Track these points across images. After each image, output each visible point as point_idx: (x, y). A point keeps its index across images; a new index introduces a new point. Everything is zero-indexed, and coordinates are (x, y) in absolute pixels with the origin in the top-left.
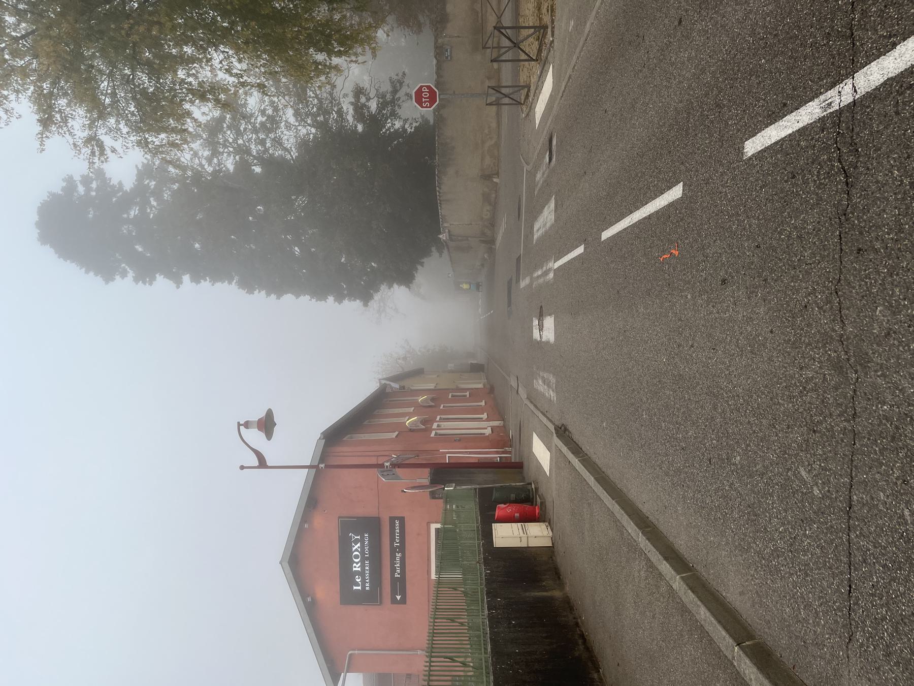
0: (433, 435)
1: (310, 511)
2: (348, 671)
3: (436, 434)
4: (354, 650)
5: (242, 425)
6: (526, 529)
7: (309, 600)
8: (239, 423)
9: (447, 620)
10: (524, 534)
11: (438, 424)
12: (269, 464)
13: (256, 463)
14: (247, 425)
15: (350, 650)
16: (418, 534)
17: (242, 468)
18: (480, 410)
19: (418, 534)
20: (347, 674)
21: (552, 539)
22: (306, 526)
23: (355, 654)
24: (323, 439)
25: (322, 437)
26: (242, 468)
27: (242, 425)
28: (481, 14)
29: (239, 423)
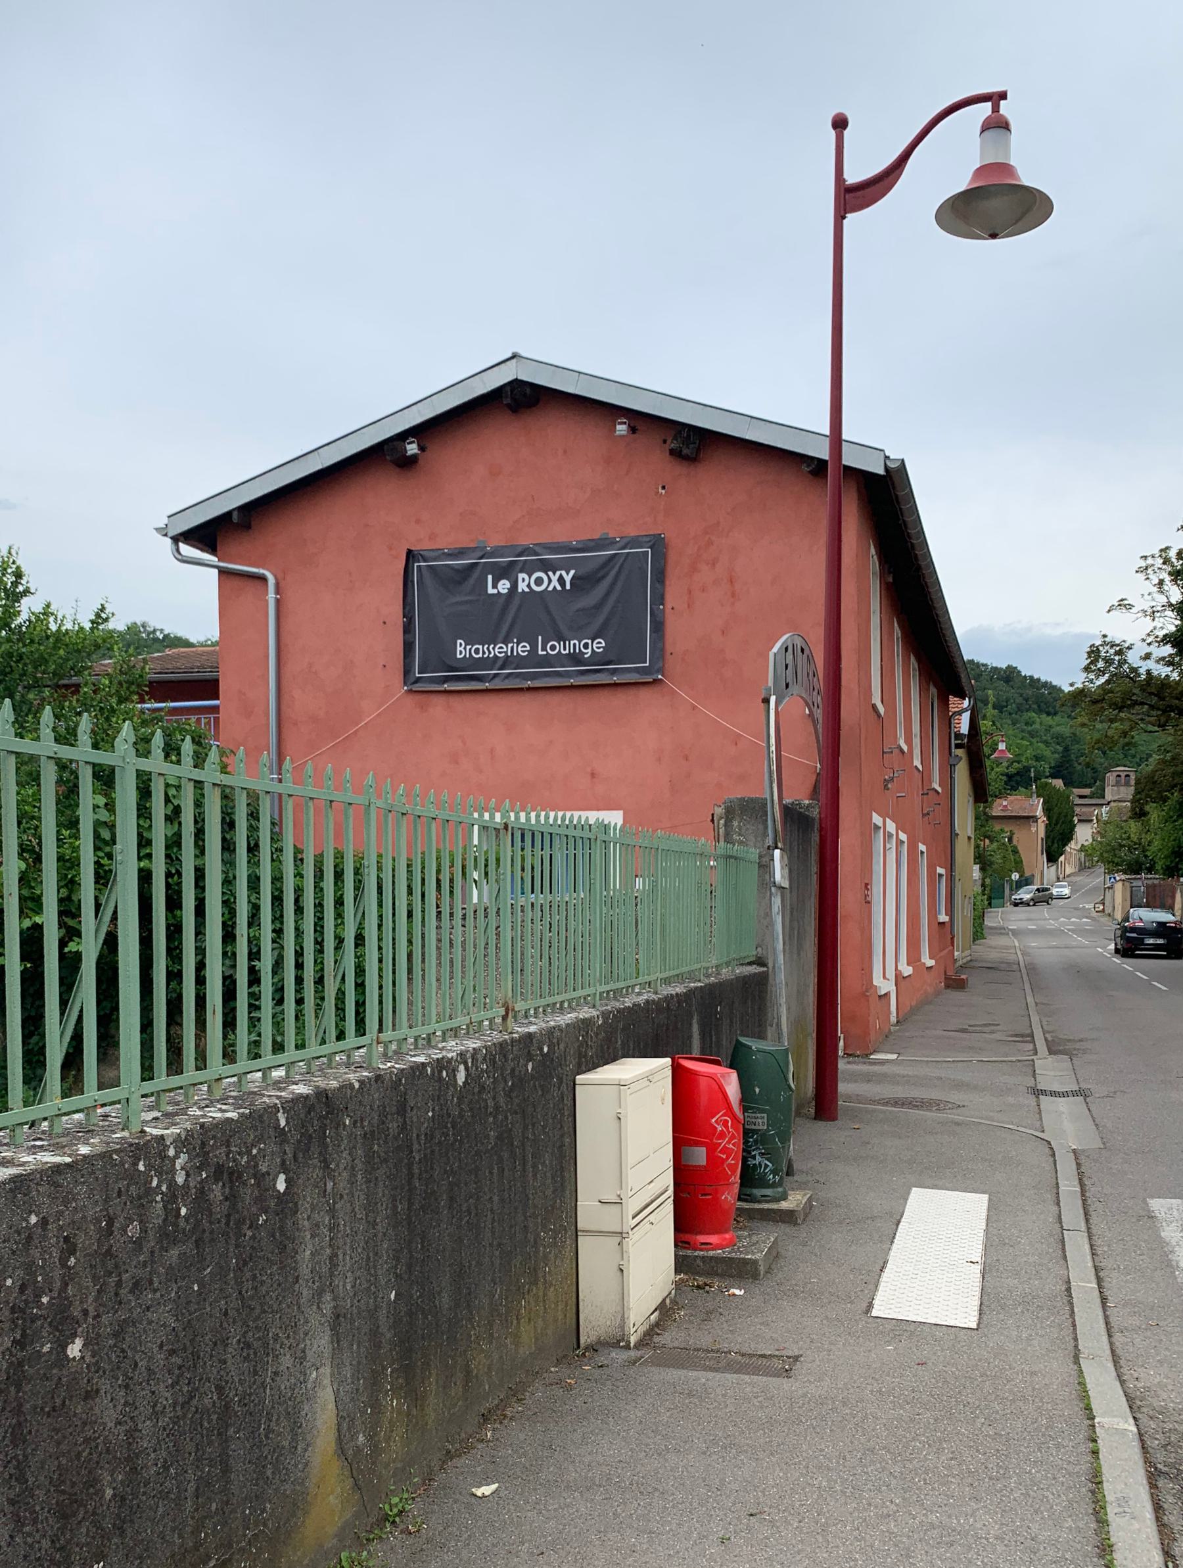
0: (877, 819)
1: (665, 442)
2: (223, 572)
3: (877, 828)
4: (278, 590)
5: (996, 109)
6: (651, 1218)
7: (409, 447)
8: (1003, 96)
9: (885, 1075)
10: (633, 1218)
11: (903, 842)
12: (851, 219)
13: (853, 176)
14: (997, 125)
15: (276, 579)
16: (593, 775)
17: (840, 124)
18: (914, 958)
19: (593, 775)
20: (216, 571)
21: (618, 1342)
22: (621, 429)
23: (267, 595)
24: (887, 468)
25: (891, 465)
26: (840, 124)
27: (996, 109)
28: (1066, 950)
29: (1003, 96)
